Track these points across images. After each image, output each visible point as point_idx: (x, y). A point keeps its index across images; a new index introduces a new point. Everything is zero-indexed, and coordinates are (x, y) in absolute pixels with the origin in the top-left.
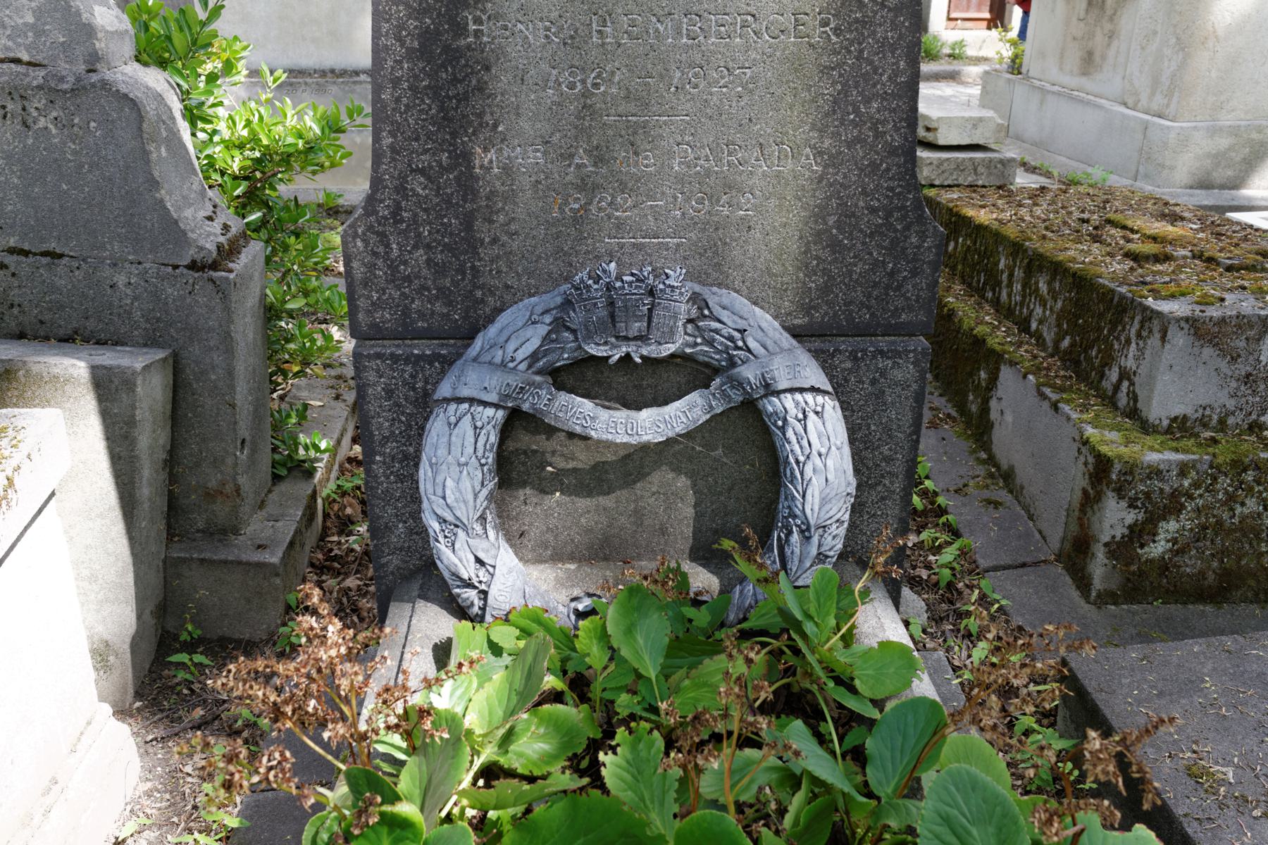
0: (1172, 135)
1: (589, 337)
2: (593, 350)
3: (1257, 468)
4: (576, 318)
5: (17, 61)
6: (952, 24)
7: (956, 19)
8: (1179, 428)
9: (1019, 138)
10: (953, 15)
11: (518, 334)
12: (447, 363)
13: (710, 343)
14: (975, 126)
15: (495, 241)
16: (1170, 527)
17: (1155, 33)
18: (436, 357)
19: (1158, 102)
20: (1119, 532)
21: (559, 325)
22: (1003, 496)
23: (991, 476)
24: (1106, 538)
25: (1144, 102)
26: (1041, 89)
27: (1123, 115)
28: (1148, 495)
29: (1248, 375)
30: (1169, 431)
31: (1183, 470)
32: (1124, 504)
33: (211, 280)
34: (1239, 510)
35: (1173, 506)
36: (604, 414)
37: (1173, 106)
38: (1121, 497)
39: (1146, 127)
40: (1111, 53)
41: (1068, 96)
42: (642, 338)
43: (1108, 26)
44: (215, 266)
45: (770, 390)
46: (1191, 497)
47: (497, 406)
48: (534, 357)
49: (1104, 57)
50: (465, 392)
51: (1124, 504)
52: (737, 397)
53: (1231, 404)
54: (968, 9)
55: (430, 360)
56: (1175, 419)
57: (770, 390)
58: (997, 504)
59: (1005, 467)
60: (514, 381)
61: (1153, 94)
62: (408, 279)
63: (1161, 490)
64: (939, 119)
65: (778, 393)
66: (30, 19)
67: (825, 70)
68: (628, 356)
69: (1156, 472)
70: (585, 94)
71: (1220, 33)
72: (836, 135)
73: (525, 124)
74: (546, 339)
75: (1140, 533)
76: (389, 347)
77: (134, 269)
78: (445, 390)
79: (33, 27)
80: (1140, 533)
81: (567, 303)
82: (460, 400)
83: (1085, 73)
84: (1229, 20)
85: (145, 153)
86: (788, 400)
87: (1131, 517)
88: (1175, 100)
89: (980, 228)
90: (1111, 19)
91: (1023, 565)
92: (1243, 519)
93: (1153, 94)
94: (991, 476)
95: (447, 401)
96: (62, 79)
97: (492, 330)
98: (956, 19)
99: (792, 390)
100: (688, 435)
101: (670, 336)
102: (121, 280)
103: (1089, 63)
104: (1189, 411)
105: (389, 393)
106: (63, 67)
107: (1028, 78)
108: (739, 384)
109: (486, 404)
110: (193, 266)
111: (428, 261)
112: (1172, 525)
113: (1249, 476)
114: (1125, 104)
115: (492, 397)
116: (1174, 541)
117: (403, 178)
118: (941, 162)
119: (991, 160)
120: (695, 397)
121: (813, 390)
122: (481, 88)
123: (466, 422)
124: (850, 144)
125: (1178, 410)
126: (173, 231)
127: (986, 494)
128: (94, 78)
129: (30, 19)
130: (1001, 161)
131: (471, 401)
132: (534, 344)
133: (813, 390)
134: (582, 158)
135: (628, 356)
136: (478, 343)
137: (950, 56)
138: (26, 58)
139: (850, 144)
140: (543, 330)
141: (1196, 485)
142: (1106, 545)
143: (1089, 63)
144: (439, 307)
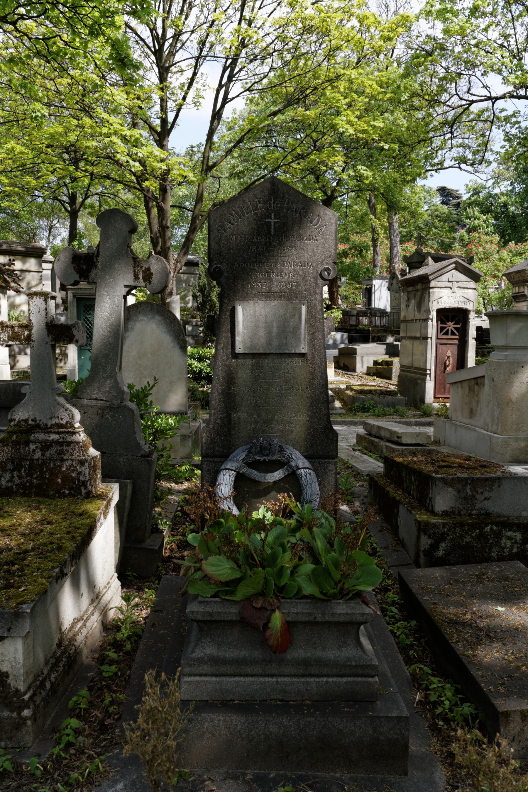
0: (500, 440)
1: (256, 455)
2: (257, 458)
3: (468, 525)
4: (253, 450)
5: (102, 400)
6: (438, 400)
7: (439, 398)
8: (445, 514)
9: (449, 446)
10: (437, 396)
11: (240, 455)
12: (222, 463)
13: (284, 457)
14: (417, 436)
15: (235, 434)
16: (443, 545)
17: (490, 401)
18: (220, 461)
19: (494, 428)
20: (427, 547)
21: (249, 452)
22: (401, 549)
23: (398, 544)
24: (422, 549)
25: (490, 428)
26: (455, 425)
27: (484, 434)
28: (434, 533)
29: (465, 497)
30: (442, 515)
31: (444, 525)
32: (426, 537)
33: (147, 460)
34: (465, 540)
35: (442, 538)
36: (259, 474)
37: (499, 429)
38: (425, 535)
39: (491, 437)
40: (479, 409)
41: (465, 427)
42: (268, 455)
43: (477, 399)
44: (148, 456)
45: (298, 468)
46: (448, 535)
47: (234, 471)
48: (243, 460)
49: (476, 411)
50: (228, 467)
51: (426, 537)
52: (291, 470)
53: (461, 507)
54: (444, 393)
55: (219, 462)
56: (443, 512)
57: (298, 468)
58: (397, 551)
59: (401, 538)
60: (239, 465)
61: (492, 425)
62: (215, 443)
63: (438, 532)
64: (402, 433)
65: (300, 469)
66: (108, 389)
67: (308, 397)
68: (265, 460)
69: (435, 526)
70: (256, 402)
71: (513, 400)
72: (311, 411)
73: (243, 408)
74: (246, 455)
75: (434, 547)
76: (209, 459)
77: (125, 457)
78: (223, 467)
79: (108, 391)
80: (434, 547)
81: (251, 447)
82: (226, 469)
83: (471, 418)
84: (516, 396)
85: (134, 424)
86: (302, 471)
87: (430, 542)
88: (500, 426)
89: (399, 463)
90: (477, 396)
91: (402, 565)
92: (467, 543)
93: (492, 425)
94: (398, 544)
95: (223, 469)
96: (114, 405)
97: (234, 454)
98: (439, 398)
99: (303, 468)
100: (279, 480)
101: (274, 454)
102: (121, 460)
103: (472, 413)
104: (448, 509)
105: (208, 470)
106: (114, 402)
107: (451, 420)
108: (291, 467)
109: (232, 470)
110: (142, 456)
111: (220, 439)
112: (444, 545)
113: (466, 528)
114: (484, 429)
115: (234, 468)
116: (445, 550)
117: (215, 420)
118: (403, 450)
119: (424, 450)
120: (280, 471)
121: (308, 468)
122: (234, 401)
123: (227, 474)
124: (315, 413)
125: (444, 508)
126: (138, 446)
127: (395, 548)
128: (123, 404)
129: (108, 389)
130: (429, 450)
131: (229, 469)
132: (244, 456)
133: (308, 468)
134: (255, 416)
135: (265, 460)
136: (231, 457)
137: (436, 415)
138: (104, 399)
139: (315, 413)
140: (245, 453)
141: (449, 530)
142: (423, 551)
143: (472, 413)
144: (221, 449)
